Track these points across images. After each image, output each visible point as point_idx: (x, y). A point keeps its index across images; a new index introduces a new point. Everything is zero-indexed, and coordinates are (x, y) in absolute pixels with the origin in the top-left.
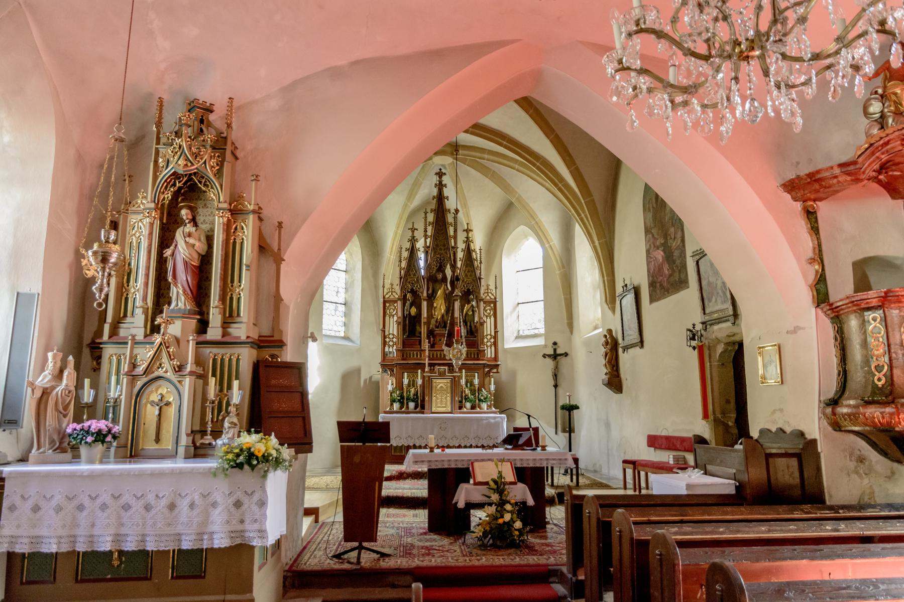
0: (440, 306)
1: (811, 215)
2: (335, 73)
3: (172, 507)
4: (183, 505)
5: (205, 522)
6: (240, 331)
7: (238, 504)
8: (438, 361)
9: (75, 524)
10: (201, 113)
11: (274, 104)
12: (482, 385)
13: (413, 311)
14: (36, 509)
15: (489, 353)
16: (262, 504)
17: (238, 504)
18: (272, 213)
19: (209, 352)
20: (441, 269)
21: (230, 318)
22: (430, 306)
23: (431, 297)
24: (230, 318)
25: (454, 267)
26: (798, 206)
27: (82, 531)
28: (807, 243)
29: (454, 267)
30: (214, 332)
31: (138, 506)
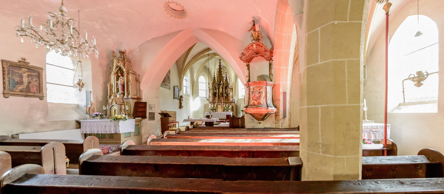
0: (221, 90)
1: (248, 66)
2: (148, 42)
3: (105, 127)
4: (107, 126)
5: (111, 129)
6: (130, 97)
7: (115, 126)
8: (219, 101)
9: (91, 129)
10: (122, 53)
11: (138, 50)
12: (228, 107)
13: (215, 91)
14: (86, 127)
15: (231, 99)
16: (119, 126)
17: (115, 126)
18: (138, 73)
19: (125, 100)
20: (220, 82)
21: (128, 94)
22: (219, 90)
23: (219, 88)
24: (128, 94)
25: (223, 81)
26: (245, 64)
27: (93, 130)
28: (247, 72)
29: (223, 81)
30: (125, 97)
31: (100, 126)
